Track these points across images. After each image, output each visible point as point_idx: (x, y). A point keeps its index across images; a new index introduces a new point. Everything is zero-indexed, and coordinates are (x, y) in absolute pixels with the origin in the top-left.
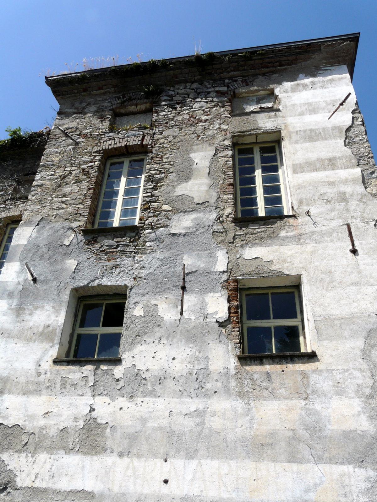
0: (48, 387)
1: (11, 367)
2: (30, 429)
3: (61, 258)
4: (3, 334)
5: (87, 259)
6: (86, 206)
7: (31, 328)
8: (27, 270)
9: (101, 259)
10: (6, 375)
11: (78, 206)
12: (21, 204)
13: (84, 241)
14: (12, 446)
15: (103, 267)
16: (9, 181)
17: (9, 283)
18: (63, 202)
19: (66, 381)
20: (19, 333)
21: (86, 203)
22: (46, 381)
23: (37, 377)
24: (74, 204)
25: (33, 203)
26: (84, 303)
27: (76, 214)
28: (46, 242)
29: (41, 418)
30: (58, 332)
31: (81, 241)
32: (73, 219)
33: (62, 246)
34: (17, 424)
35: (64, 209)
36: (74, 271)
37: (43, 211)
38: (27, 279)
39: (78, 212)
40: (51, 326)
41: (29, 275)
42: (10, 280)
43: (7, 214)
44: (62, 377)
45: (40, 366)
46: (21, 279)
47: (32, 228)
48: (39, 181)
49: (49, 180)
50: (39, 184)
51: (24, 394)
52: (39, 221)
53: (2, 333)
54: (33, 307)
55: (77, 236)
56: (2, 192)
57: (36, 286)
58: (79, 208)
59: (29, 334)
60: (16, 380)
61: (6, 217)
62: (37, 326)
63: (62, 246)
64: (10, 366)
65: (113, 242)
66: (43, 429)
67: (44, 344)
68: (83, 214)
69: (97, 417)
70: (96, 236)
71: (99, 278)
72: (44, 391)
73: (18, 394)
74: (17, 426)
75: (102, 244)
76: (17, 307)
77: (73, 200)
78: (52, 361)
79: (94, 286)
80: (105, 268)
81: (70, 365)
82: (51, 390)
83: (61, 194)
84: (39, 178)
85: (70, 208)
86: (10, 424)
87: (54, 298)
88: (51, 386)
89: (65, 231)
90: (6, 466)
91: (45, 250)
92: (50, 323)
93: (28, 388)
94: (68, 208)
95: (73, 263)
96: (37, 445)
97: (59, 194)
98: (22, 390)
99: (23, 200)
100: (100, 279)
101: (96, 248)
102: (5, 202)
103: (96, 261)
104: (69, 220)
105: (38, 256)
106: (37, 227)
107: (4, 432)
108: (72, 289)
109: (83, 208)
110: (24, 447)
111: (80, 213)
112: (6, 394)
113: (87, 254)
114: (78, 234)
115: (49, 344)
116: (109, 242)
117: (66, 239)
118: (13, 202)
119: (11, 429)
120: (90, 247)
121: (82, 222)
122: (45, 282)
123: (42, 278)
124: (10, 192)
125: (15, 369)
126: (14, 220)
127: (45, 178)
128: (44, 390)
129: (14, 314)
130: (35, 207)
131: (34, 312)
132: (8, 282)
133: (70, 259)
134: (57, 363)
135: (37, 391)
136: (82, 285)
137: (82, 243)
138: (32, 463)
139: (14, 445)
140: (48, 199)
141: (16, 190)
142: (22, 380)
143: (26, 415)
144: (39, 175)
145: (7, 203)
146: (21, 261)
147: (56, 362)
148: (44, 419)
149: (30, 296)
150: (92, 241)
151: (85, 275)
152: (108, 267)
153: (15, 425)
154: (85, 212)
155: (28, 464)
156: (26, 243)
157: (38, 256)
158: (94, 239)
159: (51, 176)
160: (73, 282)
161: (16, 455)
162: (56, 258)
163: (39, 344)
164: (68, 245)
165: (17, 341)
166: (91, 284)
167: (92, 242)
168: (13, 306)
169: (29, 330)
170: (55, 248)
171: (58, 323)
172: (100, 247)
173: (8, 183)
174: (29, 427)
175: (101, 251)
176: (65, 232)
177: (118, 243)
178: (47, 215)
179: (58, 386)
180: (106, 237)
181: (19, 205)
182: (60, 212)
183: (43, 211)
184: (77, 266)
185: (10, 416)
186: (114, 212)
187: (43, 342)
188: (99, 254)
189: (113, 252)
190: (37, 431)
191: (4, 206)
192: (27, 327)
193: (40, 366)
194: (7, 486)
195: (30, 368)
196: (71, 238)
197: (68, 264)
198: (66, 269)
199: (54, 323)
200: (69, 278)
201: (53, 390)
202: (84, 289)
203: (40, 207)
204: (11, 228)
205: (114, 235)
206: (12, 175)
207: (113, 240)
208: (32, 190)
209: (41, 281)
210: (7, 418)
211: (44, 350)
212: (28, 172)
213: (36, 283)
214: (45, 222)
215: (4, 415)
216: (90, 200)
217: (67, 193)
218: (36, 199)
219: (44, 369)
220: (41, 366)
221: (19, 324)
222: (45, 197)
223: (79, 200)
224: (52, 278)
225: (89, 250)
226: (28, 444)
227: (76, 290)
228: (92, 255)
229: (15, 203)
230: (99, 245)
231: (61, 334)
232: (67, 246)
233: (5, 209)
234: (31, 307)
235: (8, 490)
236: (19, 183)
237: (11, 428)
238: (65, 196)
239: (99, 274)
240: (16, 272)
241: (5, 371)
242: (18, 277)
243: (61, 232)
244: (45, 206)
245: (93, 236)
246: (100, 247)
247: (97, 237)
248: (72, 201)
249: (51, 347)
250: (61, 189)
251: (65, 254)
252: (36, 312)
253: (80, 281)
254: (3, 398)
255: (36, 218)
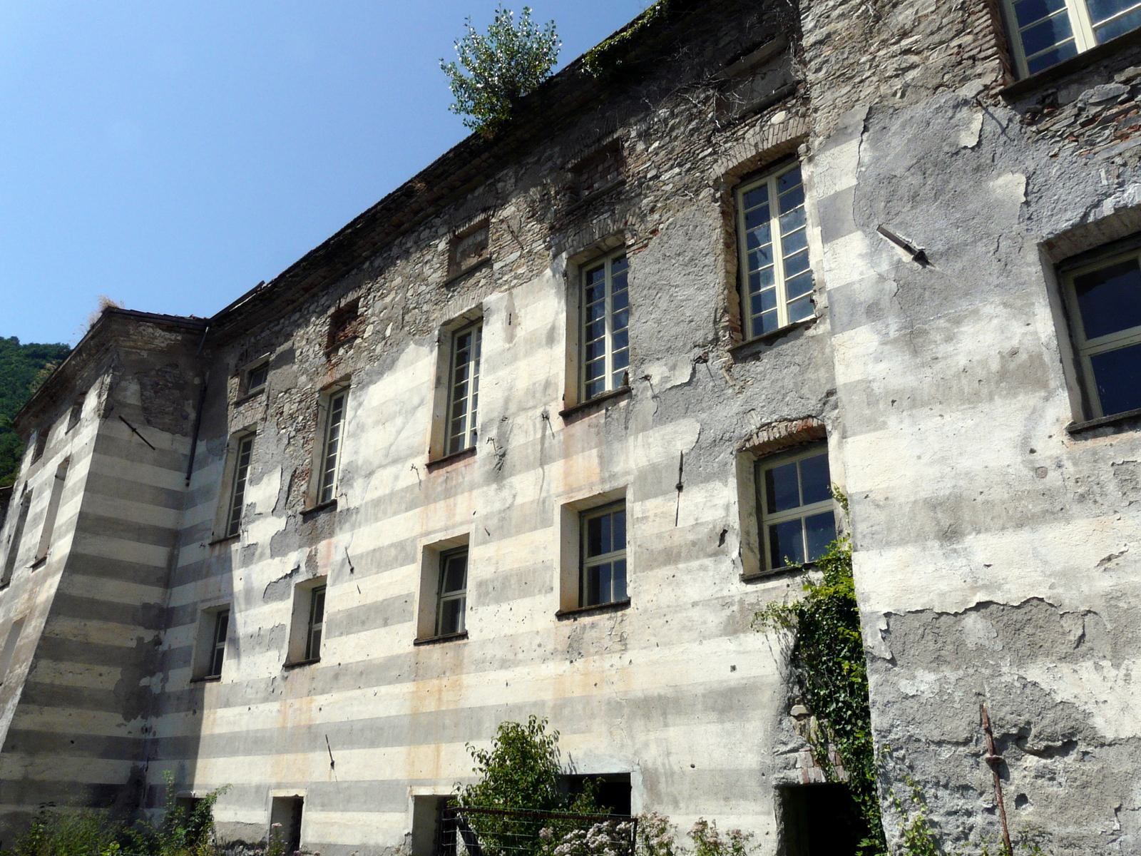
0: (1082, 498)
1: (954, 472)
2: (1078, 604)
3: (972, 183)
4: (895, 404)
5: (1048, 158)
6: (981, 31)
7: (965, 371)
8: (889, 241)
9: (1093, 144)
10: (947, 492)
11: (955, 43)
12: (748, 130)
13: (1018, 117)
14: (1042, 649)
15: (1110, 161)
16: (697, 91)
17: (857, 286)
18: (907, 52)
19: (1133, 472)
20: (937, 390)
21: (977, 24)
22: (1071, 483)
23: (1037, 480)
24: (941, 43)
25: (827, 86)
26: (1076, 274)
27: (960, 63)
28: (909, 161)
29: (1097, 573)
30: (1051, 358)
31: (1010, 120)
32: (958, 79)
33: (957, 153)
34: (1034, 598)
35: (918, 66)
36: (1024, 199)
37: (862, 95)
38: (900, 261)
39: (966, 56)
40: (1021, 350)
41: (899, 251)
42: (856, 277)
43: (725, 164)
44: (1113, 464)
45: (1032, 451)
46: (885, 267)
47: (855, 142)
48: (817, 31)
49: (842, 15)
50: (819, 38)
51: (1020, 525)
52: (865, 120)
53: (893, 402)
54: (949, 321)
55: (992, 115)
56: (694, 123)
57: (931, 271)
58: (960, 46)
59: (967, 385)
60: (980, 499)
61: (727, 173)
62: (979, 362)
63: (957, 153)
64: (950, 469)
65: (1112, 85)
66: (1118, 598)
67: (1021, 397)
68: (982, 55)
69: (225, 789)
70: (1050, 92)
71: (1112, 191)
72: (1076, 508)
73: (1003, 528)
74: (1035, 602)
75: (1079, 105)
76: (902, 332)
77: (932, 33)
78: (1065, 432)
79: (1104, 218)
80: (1118, 160)
81: (1127, 431)
82: (1095, 502)
83: (893, 36)
84: (812, 24)
85: (935, 55)
86: (1012, 601)
87: (996, 282)
88: (1089, 492)
89: (950, 113)
90: (1049, 694)
91: (916, 180)
92: (1015, 343)
93: (1024, 510)
94: (927, 58)
95: (1011, 181)
96: (1116, 637)
97: (884, 37)
98: (1011, 518)
99: (750, 121)
100: (1117, 195)
101: (1066, 122)
102: (709, 140)
103: (1080, 155)
104: (947, 86)
105: (901, 199)
106: (866, 135)
107: (1005, 621)
108: (1038, 245)
109: (975, 41)
110: (1077, 646)
111: (970, 58)
112: (969, 534)
113: (1043, 146)
114: (991, 109)
115: (1037, 394)
116: (1093, 93)
117: (963, 134)
118: (728, 134)
119: (1023, 611)
120: (1042, 126)
121: (989, 72)
122: (951, 252)
123: (939, 246)
124: (710, 116)
125: (967, 474)
126: (745, 172)
127: (828, 17)
128: (1074, 507)
129: (904, 352)
130: (837, 94)
131: (955, 331)
132: (853, 283)
133: (999, 175)
134: (1083, 434)
135: (1053, 513)
136: (1064, 225)
137: (1015, 126)
138: (1121, 683)
139: (1048, 644)
140: (862, 61)
141: (722, 106)
142: (998, 494)
143: (1048, 573)
144: (810, 18)
145: (714, 142)
146: (863, 226)
147: (1076, 432)
148: (1107, 575)
149: (927, 298)
150: (1043, 109)
151: (1063, 197)
152: (1127, 154)
153: (1028, 601)
154: (985, 47)
155: (1109, 684)
156: (854, 182)
157: (901, 199)
158: (1048, 101)
159: (843, 7)
160: (1034, 227)
161: (1065, 668)
162: (956, 186)
163: (1008, 402)
164: (975, 143)
165: (941, 410)
166: (1092, 215)
167: (1045, 111)
168: (893, 334)
169: (963, 375)
170: (941, 166)
171: (1039, 339)
172: (1077, 116)
173: (698, 97)
174: (1071, 598)
175: (1083, 125)
176: (951, 118)
177: (1134, 83)
178: (877, 100)
179: (1112, 487)
180: (1083, 82)
181: (744, 134)
182: (911, 77)
183: (862, 95)
184: (1028, 184)
185: (1002, 582)
186: (1064, 19)
187: (1015, 395)
188: (1083, 134)
189: (1126, 112)
190: (1098, 605)
191: (710, 150)
192: (954, 370)
193: (1032, 451)
194: (1074, 739)
195: (1008, 463)
196: (976, 126)
197: (998, 191)
198: (999, 204)
199: (1025, 341)
200: (1017, 222)
201: (1101, 502)
202: (1074, 235)
203: (848, 88)
204: (744, 194)
205: (1105, 67)
206: (699, 76)
207: (1110, 79)
208: (807, 59)
209: (942, 255)
210: (999, 587)
211: (1029, 411)
212: (732, 55)
213: (928, 263)
214: (880, 116)
215: (986, 582)
216: (985, 12)
217: (906, 27)
218: (828, 74)
219: (1050, 457)
220: (1039, 452)
221: (928, 371)
222: (852, 61)
223: (950, 26)
224: (969, 237)
225: (1046, 135)
226: (1087, 638)
227: (1048, 246)
228: (1061, 144)
229: (733, 134)
230: (1069, 111)
231: (1061, 362)
232: (973, 149)
233: (715, 157)
234: (942, 321)
235: (1082, 747)
236: (722, 87)
237: (1018, 607)
238: (904, 34)
239: (1105, 182)
240: (860, 255)
241: (941, 485)
242: (873, 265)
243: (939, 121)
244: (862, 81)
245: (1039, 96)
246: (1077, 116)
247: (1053, 93)
248: (931, 37)
249: (1047, 399)
250: (885, 24)
251: (977, 169)
252: (963, 329)
253: (1054, 218)
254: (966, 545)
255: (853, 116)
